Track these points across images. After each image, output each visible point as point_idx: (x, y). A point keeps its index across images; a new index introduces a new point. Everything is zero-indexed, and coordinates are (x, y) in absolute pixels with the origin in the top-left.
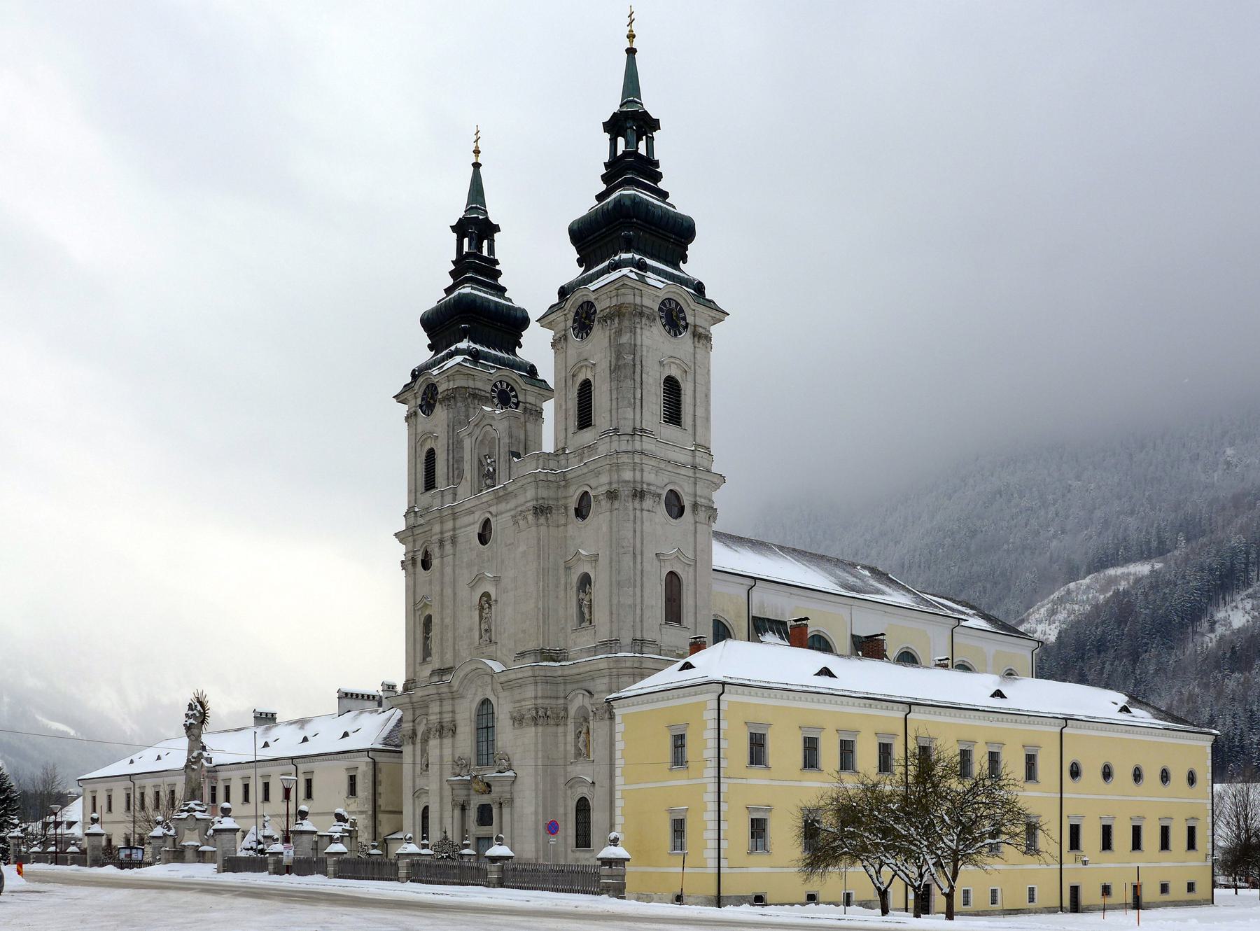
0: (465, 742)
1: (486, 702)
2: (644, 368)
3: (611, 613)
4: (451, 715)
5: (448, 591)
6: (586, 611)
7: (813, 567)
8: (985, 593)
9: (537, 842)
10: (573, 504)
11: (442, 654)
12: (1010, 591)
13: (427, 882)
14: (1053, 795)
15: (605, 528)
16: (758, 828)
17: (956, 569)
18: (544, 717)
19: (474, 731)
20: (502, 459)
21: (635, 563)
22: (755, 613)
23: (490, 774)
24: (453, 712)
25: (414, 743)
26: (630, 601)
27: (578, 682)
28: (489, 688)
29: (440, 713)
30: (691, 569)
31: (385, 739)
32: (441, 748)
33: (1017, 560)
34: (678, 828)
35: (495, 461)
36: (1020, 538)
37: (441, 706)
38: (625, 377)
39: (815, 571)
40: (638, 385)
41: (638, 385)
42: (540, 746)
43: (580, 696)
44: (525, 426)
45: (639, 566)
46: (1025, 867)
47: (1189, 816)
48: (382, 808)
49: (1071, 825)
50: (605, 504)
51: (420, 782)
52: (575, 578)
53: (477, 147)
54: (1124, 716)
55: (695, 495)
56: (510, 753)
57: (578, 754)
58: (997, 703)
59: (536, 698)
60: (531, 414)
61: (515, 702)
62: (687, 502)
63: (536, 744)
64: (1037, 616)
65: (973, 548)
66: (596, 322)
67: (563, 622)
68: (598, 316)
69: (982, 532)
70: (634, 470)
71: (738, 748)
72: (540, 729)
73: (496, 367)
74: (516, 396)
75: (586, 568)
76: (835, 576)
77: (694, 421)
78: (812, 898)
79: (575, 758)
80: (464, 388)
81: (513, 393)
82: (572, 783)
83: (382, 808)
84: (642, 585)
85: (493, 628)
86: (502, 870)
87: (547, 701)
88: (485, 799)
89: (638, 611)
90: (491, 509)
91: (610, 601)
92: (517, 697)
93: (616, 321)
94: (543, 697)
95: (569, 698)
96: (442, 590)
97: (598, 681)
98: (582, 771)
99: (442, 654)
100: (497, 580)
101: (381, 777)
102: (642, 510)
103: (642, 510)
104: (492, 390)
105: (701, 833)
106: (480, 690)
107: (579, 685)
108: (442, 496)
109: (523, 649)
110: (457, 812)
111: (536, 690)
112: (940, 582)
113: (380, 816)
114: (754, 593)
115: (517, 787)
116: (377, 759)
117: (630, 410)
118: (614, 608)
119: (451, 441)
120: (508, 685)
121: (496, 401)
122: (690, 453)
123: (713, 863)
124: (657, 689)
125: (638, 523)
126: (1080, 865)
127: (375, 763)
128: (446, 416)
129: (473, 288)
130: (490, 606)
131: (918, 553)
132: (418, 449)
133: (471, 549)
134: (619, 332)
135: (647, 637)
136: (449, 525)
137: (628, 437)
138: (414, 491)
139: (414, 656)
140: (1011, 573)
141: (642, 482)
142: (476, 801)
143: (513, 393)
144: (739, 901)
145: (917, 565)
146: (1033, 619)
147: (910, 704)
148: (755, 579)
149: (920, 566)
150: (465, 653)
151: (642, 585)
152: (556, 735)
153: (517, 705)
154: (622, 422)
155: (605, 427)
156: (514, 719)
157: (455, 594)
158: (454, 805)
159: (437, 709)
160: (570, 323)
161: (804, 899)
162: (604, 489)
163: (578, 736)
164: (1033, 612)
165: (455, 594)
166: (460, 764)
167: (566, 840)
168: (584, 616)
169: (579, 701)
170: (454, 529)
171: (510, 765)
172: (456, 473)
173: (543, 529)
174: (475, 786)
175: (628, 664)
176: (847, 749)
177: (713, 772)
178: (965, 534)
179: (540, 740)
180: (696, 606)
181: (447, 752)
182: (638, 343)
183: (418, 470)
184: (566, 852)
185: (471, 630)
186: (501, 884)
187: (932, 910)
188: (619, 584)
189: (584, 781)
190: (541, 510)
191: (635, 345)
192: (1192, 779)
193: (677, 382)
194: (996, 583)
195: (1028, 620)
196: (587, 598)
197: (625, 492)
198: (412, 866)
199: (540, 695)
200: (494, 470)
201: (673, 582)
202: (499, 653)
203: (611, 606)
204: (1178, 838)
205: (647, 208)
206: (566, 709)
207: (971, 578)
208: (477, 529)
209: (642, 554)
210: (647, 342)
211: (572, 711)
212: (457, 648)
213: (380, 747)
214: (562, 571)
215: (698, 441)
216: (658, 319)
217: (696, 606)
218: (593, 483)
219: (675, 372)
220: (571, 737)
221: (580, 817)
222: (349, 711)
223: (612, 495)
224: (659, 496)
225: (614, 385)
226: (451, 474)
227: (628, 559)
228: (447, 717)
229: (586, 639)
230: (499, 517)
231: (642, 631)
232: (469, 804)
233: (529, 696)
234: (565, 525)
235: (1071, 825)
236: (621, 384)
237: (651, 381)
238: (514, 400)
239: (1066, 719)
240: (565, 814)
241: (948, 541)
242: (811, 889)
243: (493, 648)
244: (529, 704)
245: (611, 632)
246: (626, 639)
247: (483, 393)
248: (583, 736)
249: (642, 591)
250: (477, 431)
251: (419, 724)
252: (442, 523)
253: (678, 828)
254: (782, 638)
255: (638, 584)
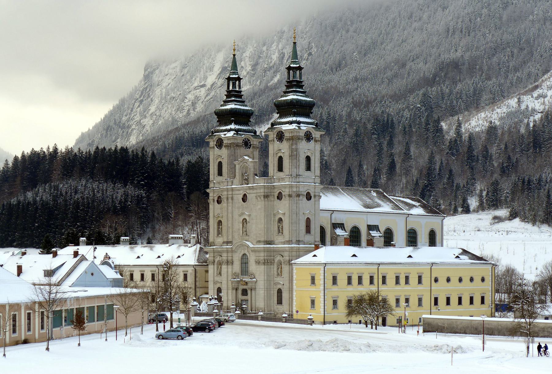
0: (237, 267)
1: (244, 254)
2: (300, 156)
3: (289, 232)
4: (231, 258)
5: (230, 215)
6: (281, 229)
7: (354, 197)
8: (512, 56)
9: (264, 303)
10: (276, 195)
11: (228, 236)
12: (532, 55)
13: (266, 321)
14: (428, 288)
15: (287, 205)
16: (335, 302)
17: (490, 36)
18: (268, 262)
19: (240, 264)
20: (251, 175)
21: (297, 217)
22: (333, 222)
23: (247, 279)
24: (232, 257)
25: (214, 265)
26: (295, 229)
27: (278, 252)
28: (246, 251)
29: (227, 257)
30: (314, 216)
31: (198, 260)
32: (227, 269)
33: (539, 30)
34: (313, 302)
35: (248, 175)
36: (543, 11)
37: (227, 254)
38: (294, 159)
39: (355, 200)
40: (298, 161)
41: (298, 161)
42: (266, 272)
43: (279, 257)
44: (253, 153)
45: (298, 218)
46: (418, 311)
47: (481, 293)
48: (198, 286)
49: (435, 298)
50: (287, 197)
51: (218, 279)
52: (277, 219)
53: (234, 48)
54: (457, 260)
55: (315, 192)
56: (254, 273)
57: (278, 275)
58: (410, 260)
59: (264, 256)
60: (255, 148)
61: (256, 256)
62: (312, 195)
63: (264, 271)
64: (548, 83)
65: (505, 18)
66: (284, 139)
67: (273, 232)
68: (285, 138)
69: (513, 4)
70: (297, 188)
71: (330, 281)
72: (266, 266)
73: (244, 134)
74: (250, 143)
75: (281, 216)
76: (361, 200)
77: (315, 168)
78: (350, 322)
79: (277, 276)
80: (234, 143)
81: (249, 142)
82: (276, 284)
83: (198, 286)
84: (299, 223)
85: (248, 230)
86: (286, 319)
87: (268, 257)
88: (245, 287)
89: (298, 232)
90: (247, 191)
91: (289, 228)
92: (257, 255)
93: (291, 141)
94: (266, 256)
95: (275, 257)
96: (227, 214)
97: (285, 253)
98: (278, 279)
99: (228, 236)
100: (249, 216)
101: (197, 275)
102: (299, 200)
103: (299, 200)
104: (243, 142)
105: (320, 303)
106: (243, 250)
107: (279, 253)
108: (227, 182)
109: (259, 240)
110: (234, 291)
111: (264, 254)
112: (477, 47)
113: (197, 290)
114: (333, 215)
115: (257, 284)
116: (196, 268)
117: (295, 169)
118: (290, 231)
119: (229, 161)
120: (254, 251)
121: (244, 145)
122: (313, 179)
123: (323, 312)
124: (307, 262)
125: (298, 204)
126: (438, 310)
127: (195, 270)
128: (227, 152)
129: (235, 104)
130: (247, 223)
131: (460, 20)
132: (215, 160)
133: (239, 203)
134: (292, 145)
135: (300, 240)
136: (230, 193)
137: (295, 178)
138: (213, 175)
139: (214, 234)
140: (534, 41)
141: (299, 191)
142: (241, 287)
143: (249, 142)
144: (330, 323)
145: (460, 30)
146: (545, 85)
147: (379, 264)
148: (333, 211)
149: (461, 31)
150: (236, 237)
151: (299, 223)
152: (270, 268)
153: (257, 257)
154: (293, 173)
155: (288, 173)
156: (256, 262)
157: (232, 216)
158: (233, 289)
159: (226, 255)
160: (275, 136)
161: (348, 322)
162: (288, 193)
163: (278, 269)
164: (546, 80)
165: (232, 216)
166: (235, 275)
167: (274, 302)
168: (280, 231)
169: (278, 258)
170: (232, 194)
171: (254, 277)
172: (231, 173)
173: (266, 202)
174: (241, 283)
175: (295, 249)
176: (360, 279)
177: (322, 288)
178: (499, 6)
179: (266, 270)
180: (315, 227)
181: (230, 270)
182: (298, 148)
183: (215, 168)
184: (274, 305)
185: (239, 230)
186: (286, 322)
187: (386, 325)
188: (292, 223)
189: (280, 283)
190: (266, 197)
191: (297, 149)
192: (483, 280)
193: (309, 157)
194: (522, 49)
195: (541, 86)
196: (281, 225)
197: (294, 195)
198: (262, 317)
199: (266, 255)
200: (248, 178)
201: (308, 221)
202: (250, 239)
203: (289, 230)
204: (477, 300)
205: (301, 103)
206: (274, 260)
207: (501, 45)
208: (241, 196)
209: (299, 214)
210: (301, 147)
211: (276, 261)
212: (233, 235)
213: (197, 264)
214: (272, 216)
215: (316, 175)
216: (304, 139)
217: (315, 227)
218: (283, 190)
219: (309, 154)
220: (275, 269)
221: (279, 294)
222: (173, 244)
223: (290, 196)
224: (304, 195)
225: (290, 160)
226: (229, 173)
227: (294, 216)
228: (230, 258)
229: (280, 239)
230: (250, 195)
231: (299, 238)
232: (238, 288)
233: (262, 256)
234: (274, 201)
235: (435, 298)
236: (292, 161)
237: (302, 159)
238: (249, 144)
239: (432, 264)
240: (274, 293)
241: (485, 11)
242: (349, 319)
243: (248, 237)
244: (262, 258)
245: (289, 238)
246: (294, 241)
247: (240, 144)
248: (280, 269)
249: (299, 225)
250: (242, 163)
251: (216, 258)
252: (227, 191)
253: (313, 302)
254: (342, 230)
255: (298, 223)
